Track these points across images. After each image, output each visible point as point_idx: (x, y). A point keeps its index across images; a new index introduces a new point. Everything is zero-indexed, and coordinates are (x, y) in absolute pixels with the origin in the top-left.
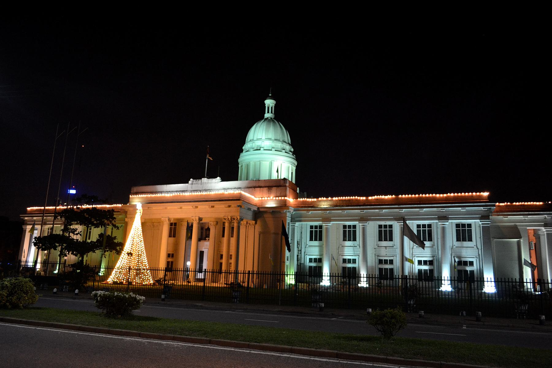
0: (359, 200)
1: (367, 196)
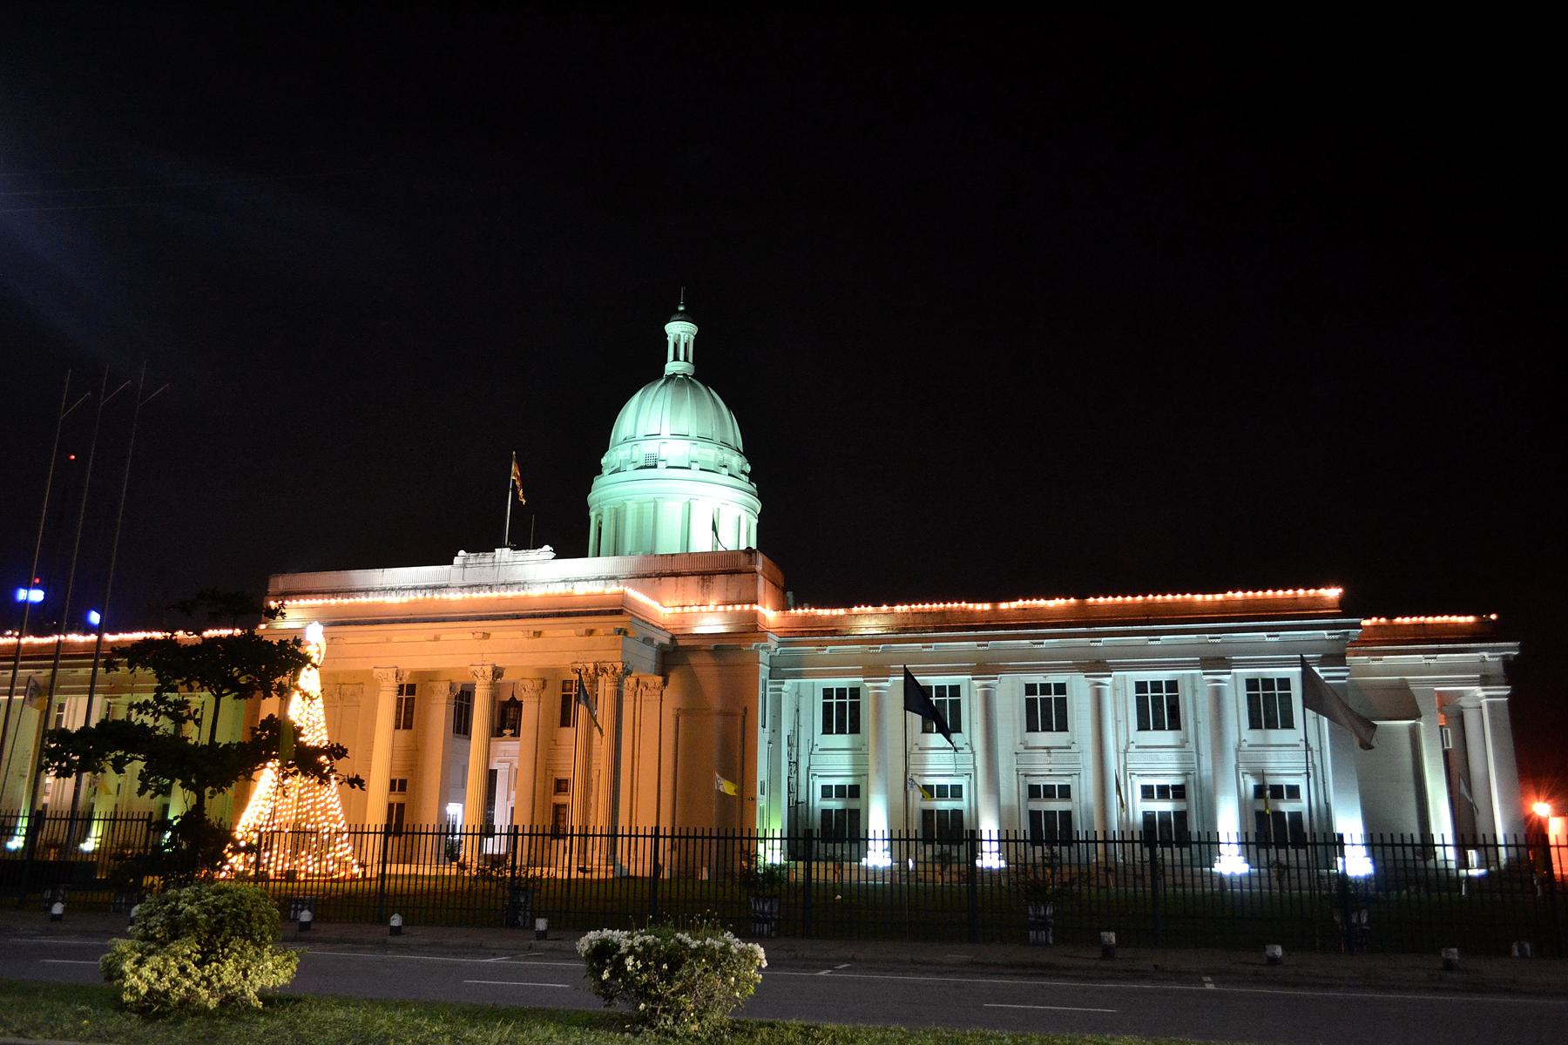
0: (973, 612)
1: (995, 599)
